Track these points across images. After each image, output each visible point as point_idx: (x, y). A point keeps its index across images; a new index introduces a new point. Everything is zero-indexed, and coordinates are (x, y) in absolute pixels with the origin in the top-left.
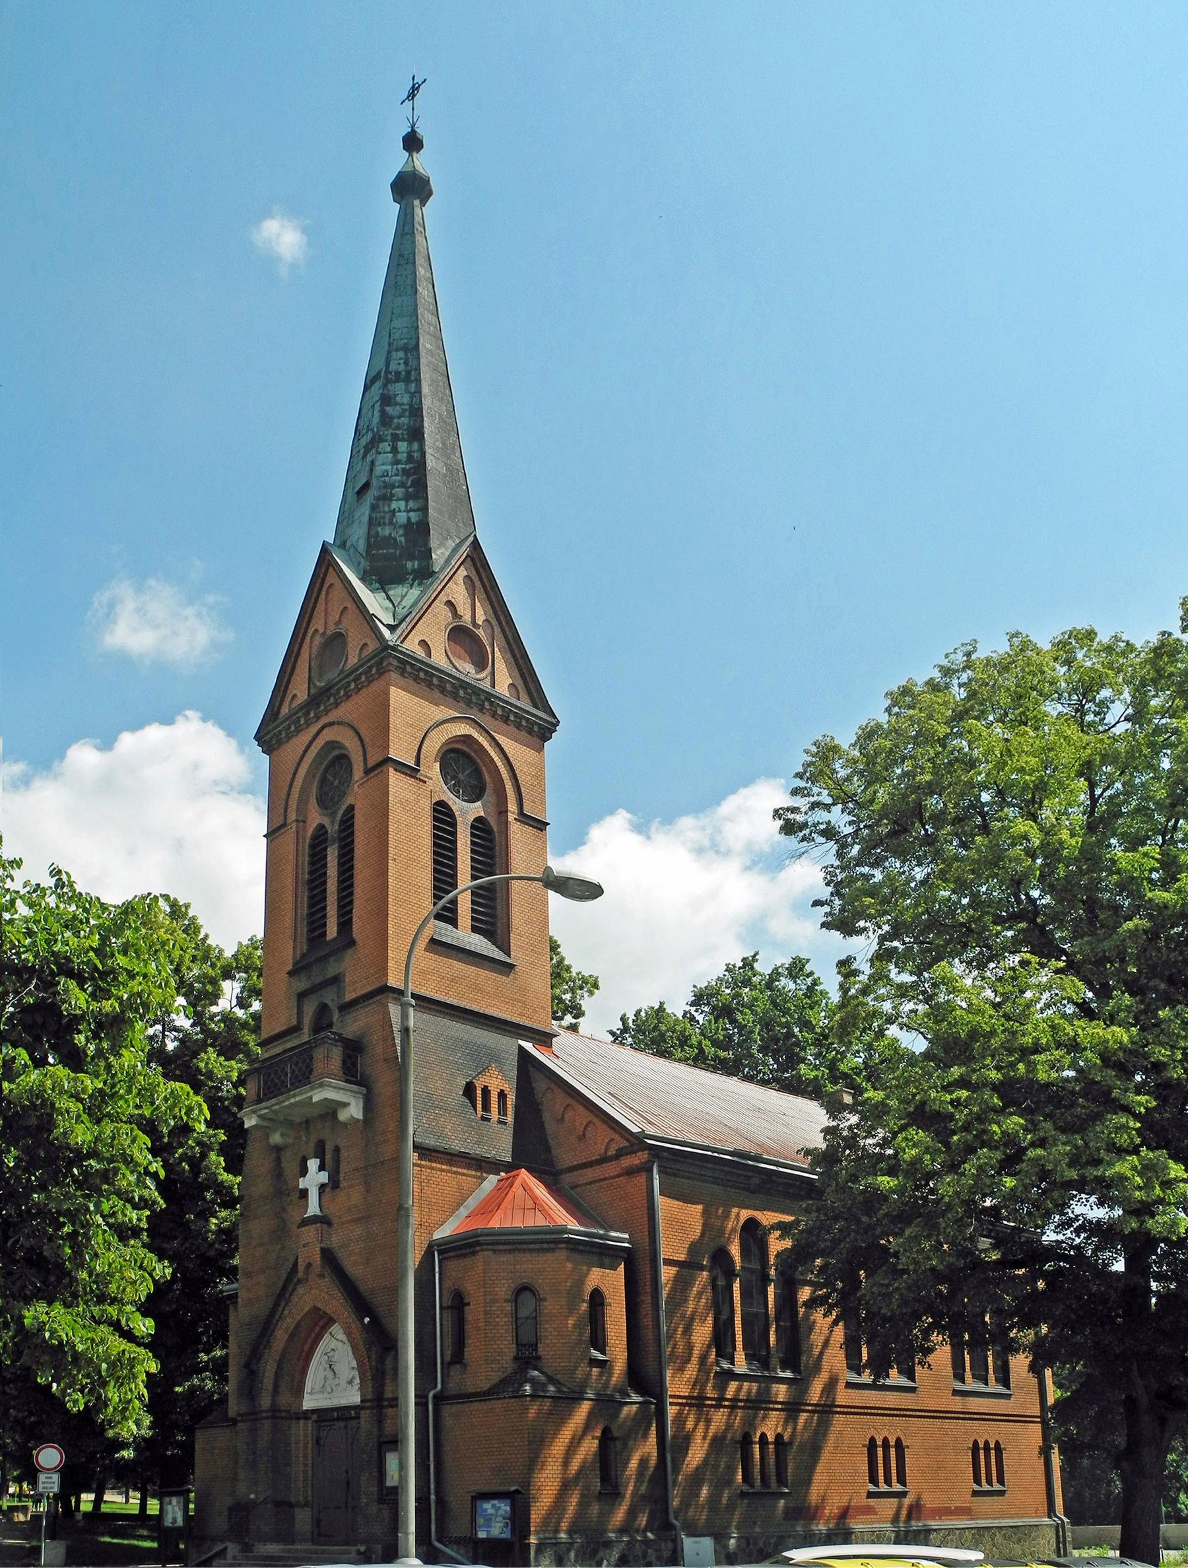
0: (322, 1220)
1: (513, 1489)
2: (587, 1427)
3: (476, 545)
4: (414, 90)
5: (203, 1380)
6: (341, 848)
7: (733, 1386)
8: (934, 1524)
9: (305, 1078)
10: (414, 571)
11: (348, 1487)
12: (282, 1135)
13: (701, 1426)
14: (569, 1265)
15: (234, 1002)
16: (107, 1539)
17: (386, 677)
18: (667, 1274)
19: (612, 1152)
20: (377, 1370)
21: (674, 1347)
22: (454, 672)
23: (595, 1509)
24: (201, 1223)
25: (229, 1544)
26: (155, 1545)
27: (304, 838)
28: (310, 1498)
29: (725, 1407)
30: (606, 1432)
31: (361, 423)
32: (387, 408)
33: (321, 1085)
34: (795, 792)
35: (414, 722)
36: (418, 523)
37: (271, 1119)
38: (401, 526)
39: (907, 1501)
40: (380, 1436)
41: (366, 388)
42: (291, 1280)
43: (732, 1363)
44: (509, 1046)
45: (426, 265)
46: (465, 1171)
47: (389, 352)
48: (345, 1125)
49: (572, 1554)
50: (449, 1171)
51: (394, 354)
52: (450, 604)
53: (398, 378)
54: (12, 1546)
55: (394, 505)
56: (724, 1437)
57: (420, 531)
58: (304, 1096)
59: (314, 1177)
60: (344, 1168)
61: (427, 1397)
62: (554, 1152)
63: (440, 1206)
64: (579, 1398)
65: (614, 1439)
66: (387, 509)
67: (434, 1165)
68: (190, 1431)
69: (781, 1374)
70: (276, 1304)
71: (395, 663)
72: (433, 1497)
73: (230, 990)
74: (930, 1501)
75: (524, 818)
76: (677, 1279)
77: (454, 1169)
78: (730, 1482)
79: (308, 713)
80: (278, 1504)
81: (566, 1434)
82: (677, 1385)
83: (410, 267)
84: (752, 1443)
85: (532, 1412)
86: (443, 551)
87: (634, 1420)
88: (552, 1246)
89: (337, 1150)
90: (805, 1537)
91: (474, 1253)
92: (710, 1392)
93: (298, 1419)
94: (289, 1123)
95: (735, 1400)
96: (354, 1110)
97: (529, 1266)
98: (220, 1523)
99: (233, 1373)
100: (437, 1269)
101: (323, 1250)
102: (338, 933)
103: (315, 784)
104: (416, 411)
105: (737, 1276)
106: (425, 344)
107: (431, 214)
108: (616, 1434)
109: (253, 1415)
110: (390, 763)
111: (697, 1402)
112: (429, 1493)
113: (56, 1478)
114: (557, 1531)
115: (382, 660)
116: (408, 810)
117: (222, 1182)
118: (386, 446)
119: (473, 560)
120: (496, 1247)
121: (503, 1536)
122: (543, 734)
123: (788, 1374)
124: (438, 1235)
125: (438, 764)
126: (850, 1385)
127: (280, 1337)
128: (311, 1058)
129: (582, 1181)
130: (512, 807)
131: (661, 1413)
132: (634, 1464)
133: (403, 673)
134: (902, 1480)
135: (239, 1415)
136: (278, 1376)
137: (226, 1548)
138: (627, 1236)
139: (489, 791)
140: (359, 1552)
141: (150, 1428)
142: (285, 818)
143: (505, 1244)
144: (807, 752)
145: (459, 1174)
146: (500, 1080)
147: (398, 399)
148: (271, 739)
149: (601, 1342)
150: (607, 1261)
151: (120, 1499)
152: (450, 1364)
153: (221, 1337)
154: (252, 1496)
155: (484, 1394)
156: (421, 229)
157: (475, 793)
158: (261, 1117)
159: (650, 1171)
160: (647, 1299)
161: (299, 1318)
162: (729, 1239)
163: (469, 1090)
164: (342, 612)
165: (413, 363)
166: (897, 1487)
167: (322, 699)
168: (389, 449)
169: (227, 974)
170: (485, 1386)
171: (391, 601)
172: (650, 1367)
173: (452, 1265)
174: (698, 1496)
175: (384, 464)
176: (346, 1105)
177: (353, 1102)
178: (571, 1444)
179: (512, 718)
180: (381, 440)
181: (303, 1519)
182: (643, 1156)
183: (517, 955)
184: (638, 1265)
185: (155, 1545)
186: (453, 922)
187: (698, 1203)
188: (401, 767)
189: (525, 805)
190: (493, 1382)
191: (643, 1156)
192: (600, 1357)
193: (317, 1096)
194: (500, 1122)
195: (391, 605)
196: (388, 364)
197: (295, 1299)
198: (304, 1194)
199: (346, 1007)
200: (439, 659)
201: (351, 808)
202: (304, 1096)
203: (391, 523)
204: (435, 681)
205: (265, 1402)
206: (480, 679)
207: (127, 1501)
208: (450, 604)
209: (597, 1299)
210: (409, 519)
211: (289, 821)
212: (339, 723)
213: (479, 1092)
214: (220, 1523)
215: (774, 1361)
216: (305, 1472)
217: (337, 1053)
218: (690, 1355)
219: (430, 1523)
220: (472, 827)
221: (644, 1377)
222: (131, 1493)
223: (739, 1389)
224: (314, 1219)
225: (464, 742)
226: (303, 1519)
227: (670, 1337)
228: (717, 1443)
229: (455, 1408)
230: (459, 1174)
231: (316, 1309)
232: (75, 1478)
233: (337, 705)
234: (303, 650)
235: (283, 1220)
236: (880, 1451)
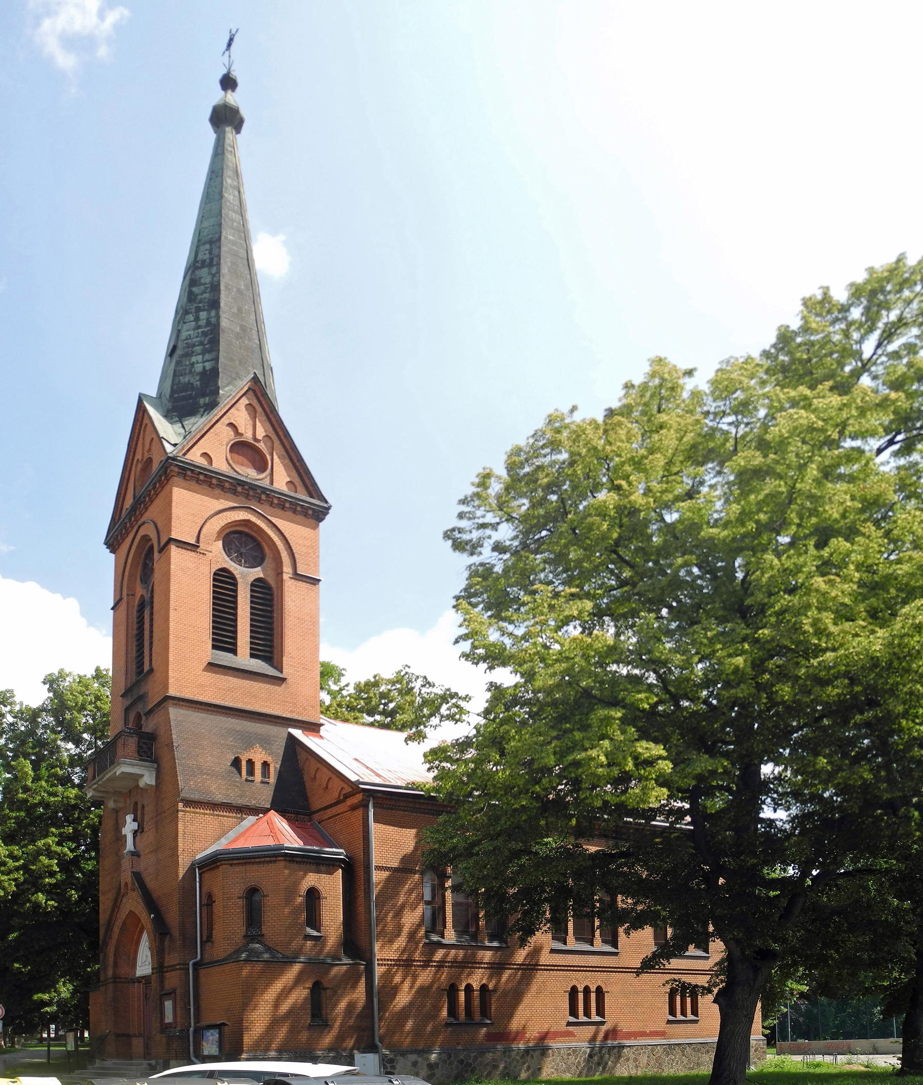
2: (298, 981)
8: (627, 1042)
10: (205, 405)
12: (115, 801)
18: (378, 877)
21: (385, 926)
22: (234, 475)
29: (432, 966)
33: (119, 764)
34: (461, 516)
36: (210, 370)
37: (104, 792)
38: (198, 374)
39: (604, 1028)
44: (279, 734)
50: (210, 814)
55: (194, 359)
59: (130, 826)
60: (146, 818)
62: (310, 801)
64: (289, 961)
69: (487, 944)
70: (113, 911)
71: (176, 469)
74: (624, 1027)
75: (297, 576)
79: (130, 519)
80: (118, 1036)
81: (278, 986)
82: (384, 953)
83: (219, 179)
86: (231, 389)
87: (343, 975)
89: (143, 807)
90: (505, 1052)
91: (218, 867)
105: (450, 877)
107: (244, 144)
110: (172, 542)
111: (406, 964)
115: (167, 468)
119: (254, 392)
120: (231, 862)
122: (318, 516)
123: (495, 944)
126: (553, 951)
130: (287, 569)
132: (343, 1005)
133: (185, 477)
134: (601, 1012)
144: (473, 484)
147: (203, 281)
149: (318, 924)
155: (223, 960)
157: (256, 559)
159: (367, 807)
160: (361, 894)
163: (236, 763)
165: (215, 252)
166: (596, 1018)
168: (192, 318)
170: (222, 955)
176: (142, 776)
182: (359, 797)
183: (287, 671)
184: (354, 871)
186: (234, 651)
187: (413, 828)
190: (229, 953)
191: (359, 797)
192: (315, 933)
194: (262, 782)
200: (220, 464)
204: (214, 481)
206: (261, 479)
209: (313, 895)
210: (204, 367)
219: (189, 1046)
220: (252, 585)
223: (446, 955)
225: (246, 525)
227: (379, 920)
236: (581, 996)
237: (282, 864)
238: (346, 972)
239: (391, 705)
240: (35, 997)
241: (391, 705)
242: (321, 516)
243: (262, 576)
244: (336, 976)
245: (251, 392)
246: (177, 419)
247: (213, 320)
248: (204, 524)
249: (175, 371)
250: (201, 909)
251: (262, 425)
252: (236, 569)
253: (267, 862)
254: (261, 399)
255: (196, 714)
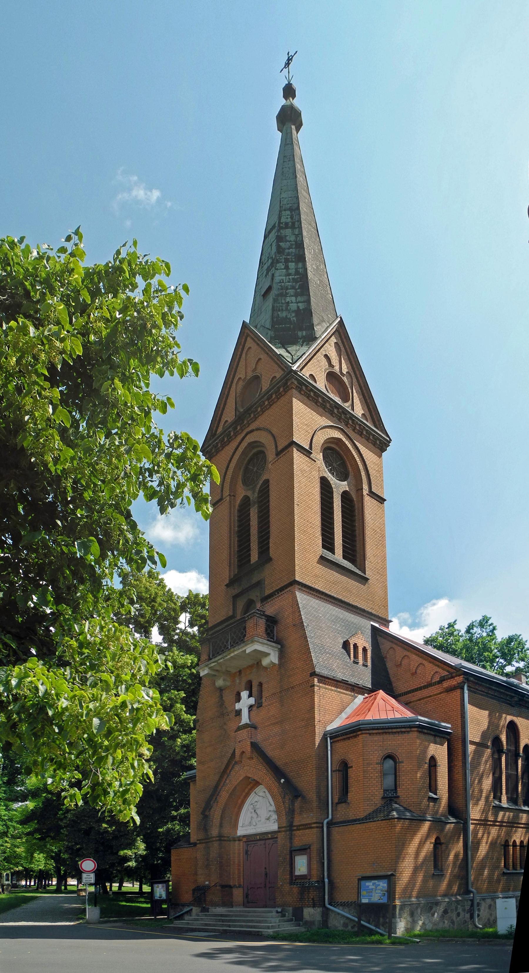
0: (252, 726)
1: (390, 873)
2: (428, 836)
3: (341, 323)
4: (289, 60)
5: (174, 825)
6: (259, 507)
7: (501, 814)
9: (241, 638)
10: (303, 337)
11: (267, 876)
12: (224, 680)
13: (486, 835)
14: (418, 741)
15: (187, 624)
16: (124, 903)
17: (289, 393)
18: (471, 748)
19: (437, 679)
20: (289, 809)
23: (431, 883)
24: (171, 742)
25: (193, 908)
26: (149, 906)
27: (234, 506)
28: (242, 883)
30: (437, 839)
31: (263, 258)
32: (281, 244)
33: (253, 642)
35: (307, 424)
36: (303, 309)
37: (217, 670)
38: (293, 311)
40: (291, 847)
41: (265, 237)
42: (232, 761)
43: (500, 802)
45: (300, 163)
46: (344, 691)
47: (280, 211)
48: (265, 668)
49: (419, 911)
50: (336, 691)
51: (283, 212)
52: (326, 356)
53: (287, 226)
54: (75, 908)
55: (288, 299)
56: (496, 842)
57: (306, 315)
58: (241, 650)
59: (246, 701)
60: (265, 694)
61: (323, 823)
63: (333, 711)
65: (441, 844)
66: (283, 301)
67: (327, 686)
68: (168, 851)
72: (326, 880)
73: (184, 618)
75: (372, 494)
76: (475, 752)
77: (339, 690)
78: (498, 867)
80: (223, 886)
82: (475, 813)
83: (292, 162)
84: (509, 846)
85: (398, 827)
88: (408, 729)
89: (260, 685)
92: (491, 818)
93: (235, 841)
94: (227, 673)
95: (502, 822)
96: (273, 658)
97: (393, 743)
98: (187, 897)
99: (194, 820)
100: (329, 748)
101: (251, 743)
102: (259, 558)
103: (241, 473)
104: (300, 245)
106: (303, 208)
108: (442, 840)
109: (207, 840)
111: (484, 823)
112: (324, 878)
113: (92, 876)
114: (410, 897)
115: (288, 380)
116: (307, 475)
117: (184, 719)
118: (281, 265)
119: (339, 333)
120: (371, 732)
121: (381, 901)
124: (329, 728)
125: (321, 454)
127: (224, 796)
128: (245, 628)
129: (414, 699)
130: (365, 487)
131: (465, 830)
132: (451, 857)
135: (198, 840)
136: (222, 818)
137: (192, 909)
138: (449, 726)
139: (351, 477)
140: (277, 912)
141: (145, 850)
142: (222, 495)
143: (378, 729)
145: (342, 693)
146: (363, 641)
147: (288, 238)
148: (211, 450)
150: (438, 739)
151: (131, 885)
152: (337, 804)
153: (186, 802)
154: (207, 883)
155: (363, 819)
156: (296, 142)
157: (343, 477)
158: (211, 668)
159: (463, 689)
161: (236, 783)
162: (501, 731)
163: (346, 645)
164: (258, 361)
165: (296, 218)
167: (244, 417)
168: (283, 267)
169: (183, 608)
170: (362, 815)
171: (289, 353)
172: (459, 802)
173: (339, 745)
174: (483, 875)
175: (280, 275)
176: (267, 655)
177: (272, 652)
178: (418, 846)
179: (364, 433)
180: (278, 262)
181: (238, 894)
182: (460, 679)
184: (455, 742)
185: (149, 906)
188: (301, 448)
189: (373, 486)
190: (368, 812)
191: (460, 679)
193: (249, 649)
194: (364, 665)
195: (290, 355)
196: (280, 218)
197: (233, 773)
198: (239, 713)
199: (265, 599)
200: (321, 384)
201: (267, 482)
202: (241, 650)
203: (287, 309)
205: (214, 832)
207: (133, 886)
208: (326, 356)
211: (224, 496)
212: (258, 429)
213: (352, 646)
214: (187, 897)
215: (520, 801)
216: (239, 870)
217: (262, 622)
218: (481, 796)
219: (324, 895)
221: (458, 810)
222: (135, 883)
223: (504, 816)
224: (246, 726)
225: (337, 444)
226: (238, 894)
228: (493, 845)
229: (341, 829)
230: (342, 693)
231: (247, 778)
232: (102, 876)
233: (256, 418)
234: (231, 392)
235: (225, 730)
237: (415, 734)
238: (454, 828)
239: (119, 664)
240: (122, 853)
241: (119, 664)
242: (384, 447)
243: (348, 489)
244: (449, 829)
245: (337, 333)
246: (280, 345)
247: (301, 270)
248: (314, 435)
249: (273, 307)
250: (331, 774)
251: (346, 365)
252: (332, 480)
253: (402, 732)
254: (345, 340)
255: (314, 600)
